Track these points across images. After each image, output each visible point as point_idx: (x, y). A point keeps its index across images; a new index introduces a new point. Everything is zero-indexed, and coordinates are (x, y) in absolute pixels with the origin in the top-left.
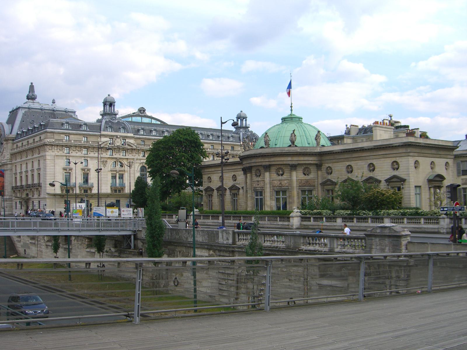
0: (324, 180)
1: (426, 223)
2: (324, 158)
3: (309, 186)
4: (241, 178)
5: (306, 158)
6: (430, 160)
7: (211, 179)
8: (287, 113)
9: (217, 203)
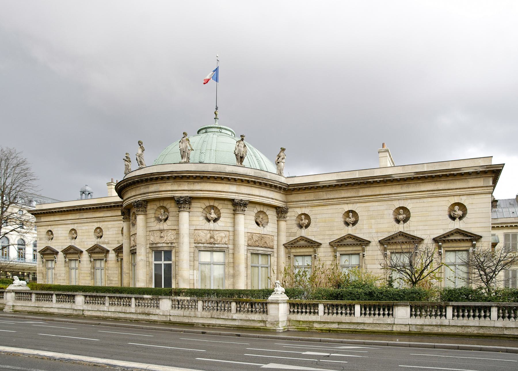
0: (292, 238)
2: (294, 197)
3: (265, 247)
4: (111, 233)
7: (52, 234)
9: (63, 275)
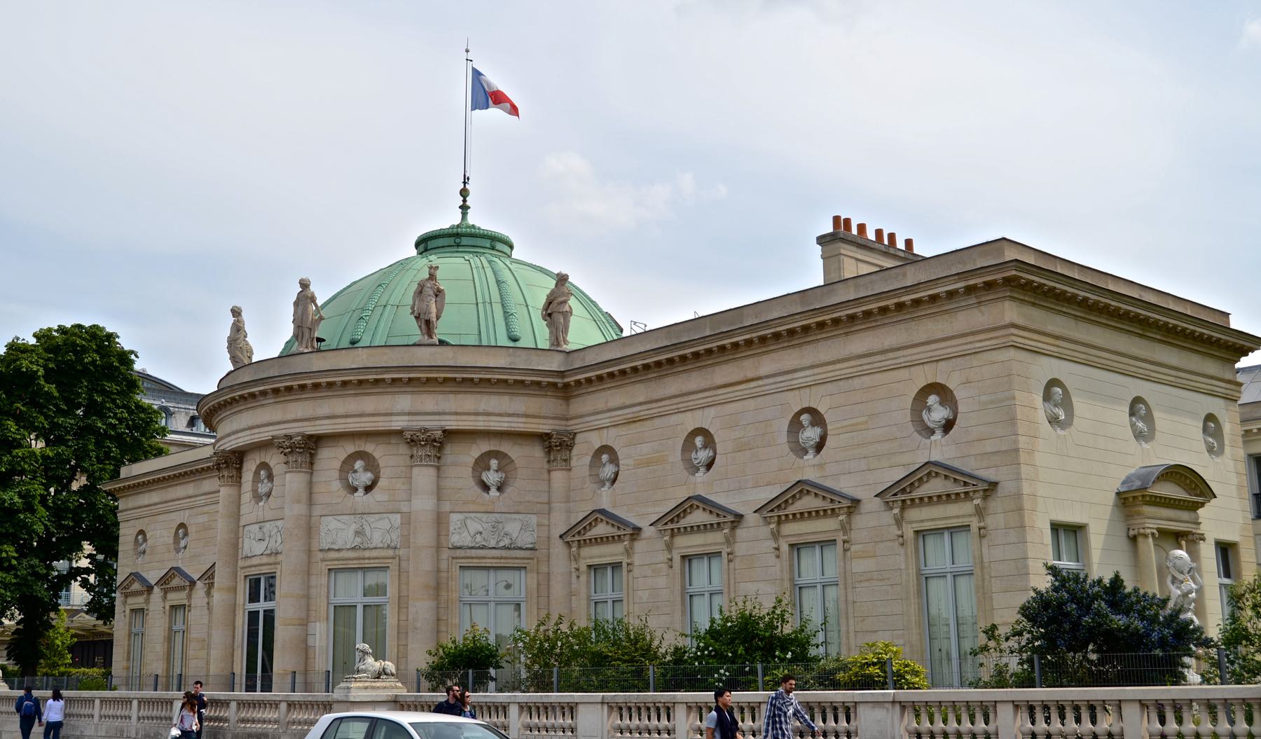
2: (586, 404)
8: (448, 219)
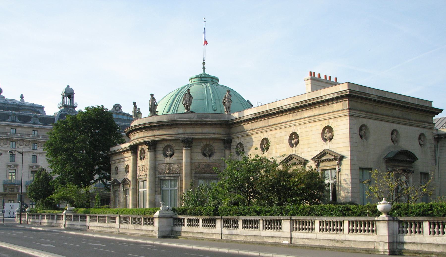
1: (353, 231)
3: (212, 173)
5: (206, 130)
6: (388, 127)
